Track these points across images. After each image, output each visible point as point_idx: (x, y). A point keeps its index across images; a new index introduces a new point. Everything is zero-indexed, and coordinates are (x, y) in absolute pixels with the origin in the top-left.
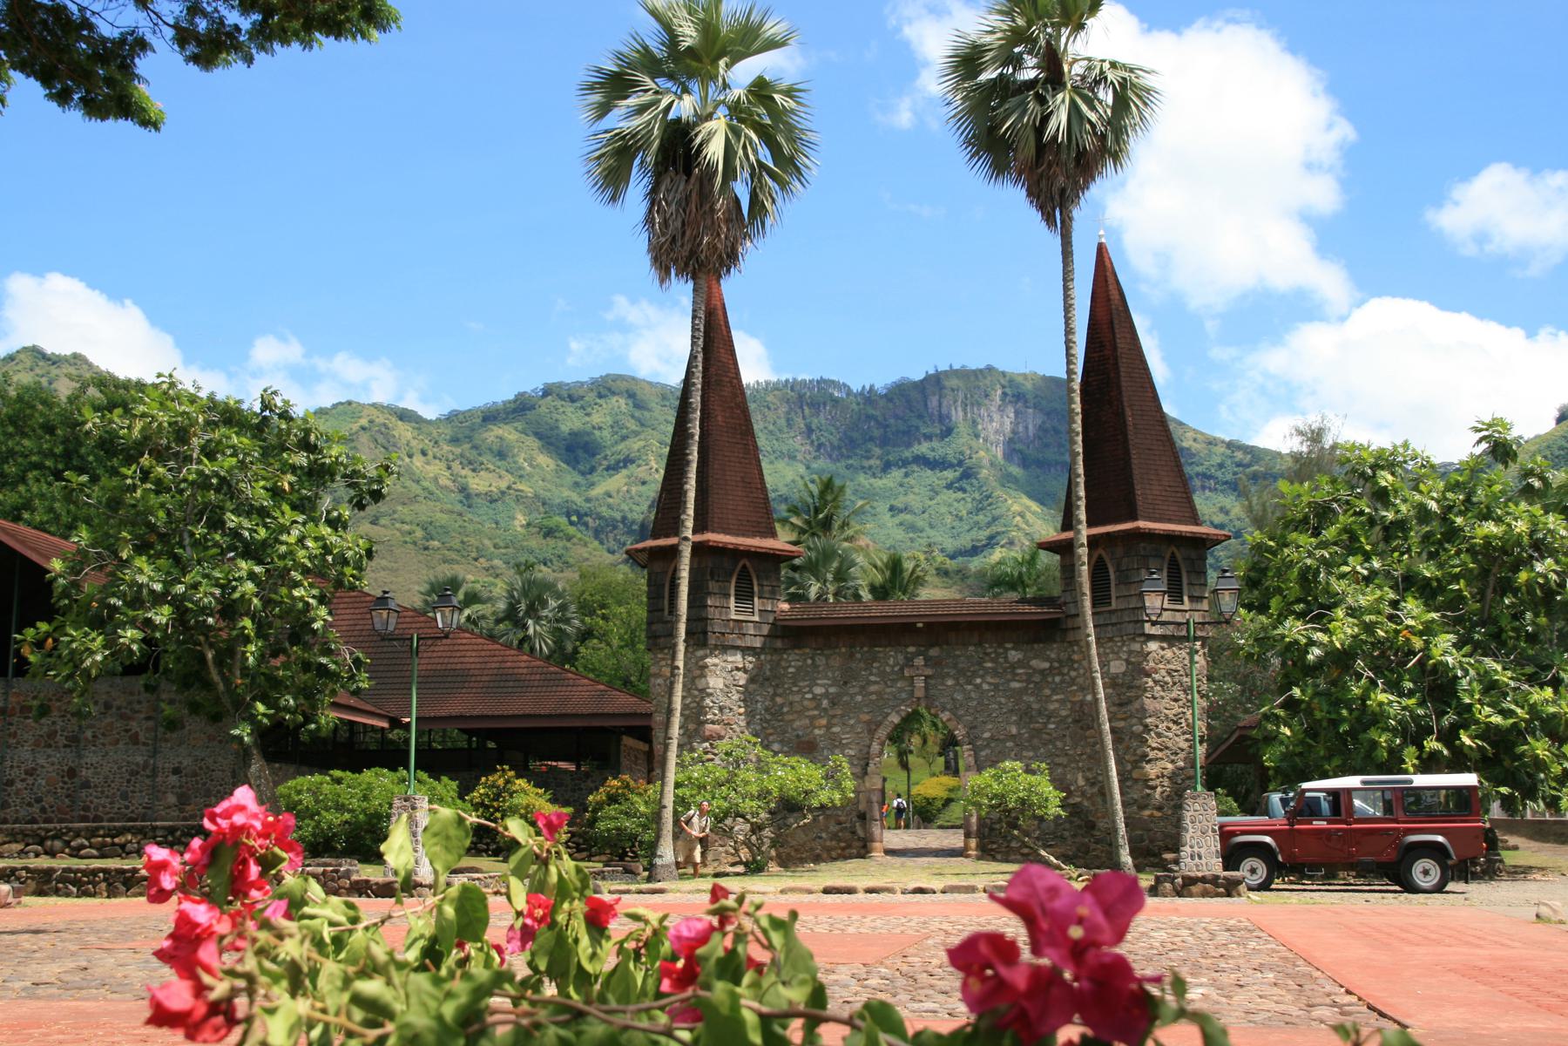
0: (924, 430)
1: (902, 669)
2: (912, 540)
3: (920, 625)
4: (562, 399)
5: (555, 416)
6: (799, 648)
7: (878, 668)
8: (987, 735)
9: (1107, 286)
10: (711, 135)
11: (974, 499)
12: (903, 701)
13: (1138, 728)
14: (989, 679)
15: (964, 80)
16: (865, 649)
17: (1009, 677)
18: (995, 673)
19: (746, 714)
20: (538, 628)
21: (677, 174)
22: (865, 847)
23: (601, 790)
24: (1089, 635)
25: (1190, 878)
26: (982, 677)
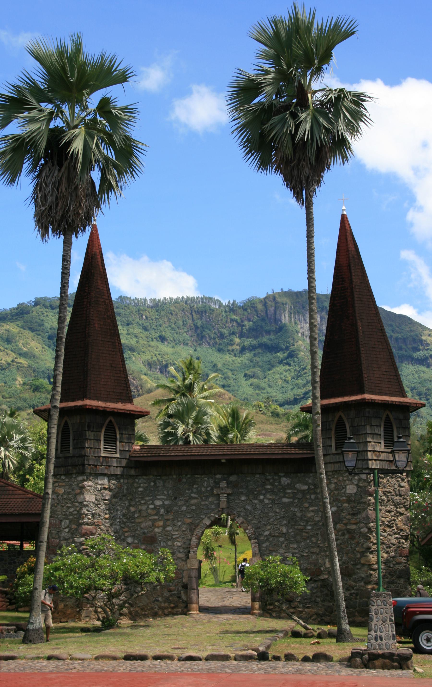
0: (268, 328)
1: (212, 489)
2: (258, 394)
3: (223, 461)
4: (46, 307)
5: (42, 318)
6: (146, 475)
7: (197, 488)
8: (267, 533)
9: (347, 242)
10: (76, 137)
11: (295, 370)
12: (213, 510)
13: (365, 530)
14: (268, 496)
15: (242, 104)
16: (189, 476)
17: (281, 495)
18: (272, 492)
19: (110, 518)
20: (7, 453)
21: (53, 166)
22: (186, 607)
23: (25, 564)
24: (321, 474)
25: (373, 654)
26: (264, 495)
